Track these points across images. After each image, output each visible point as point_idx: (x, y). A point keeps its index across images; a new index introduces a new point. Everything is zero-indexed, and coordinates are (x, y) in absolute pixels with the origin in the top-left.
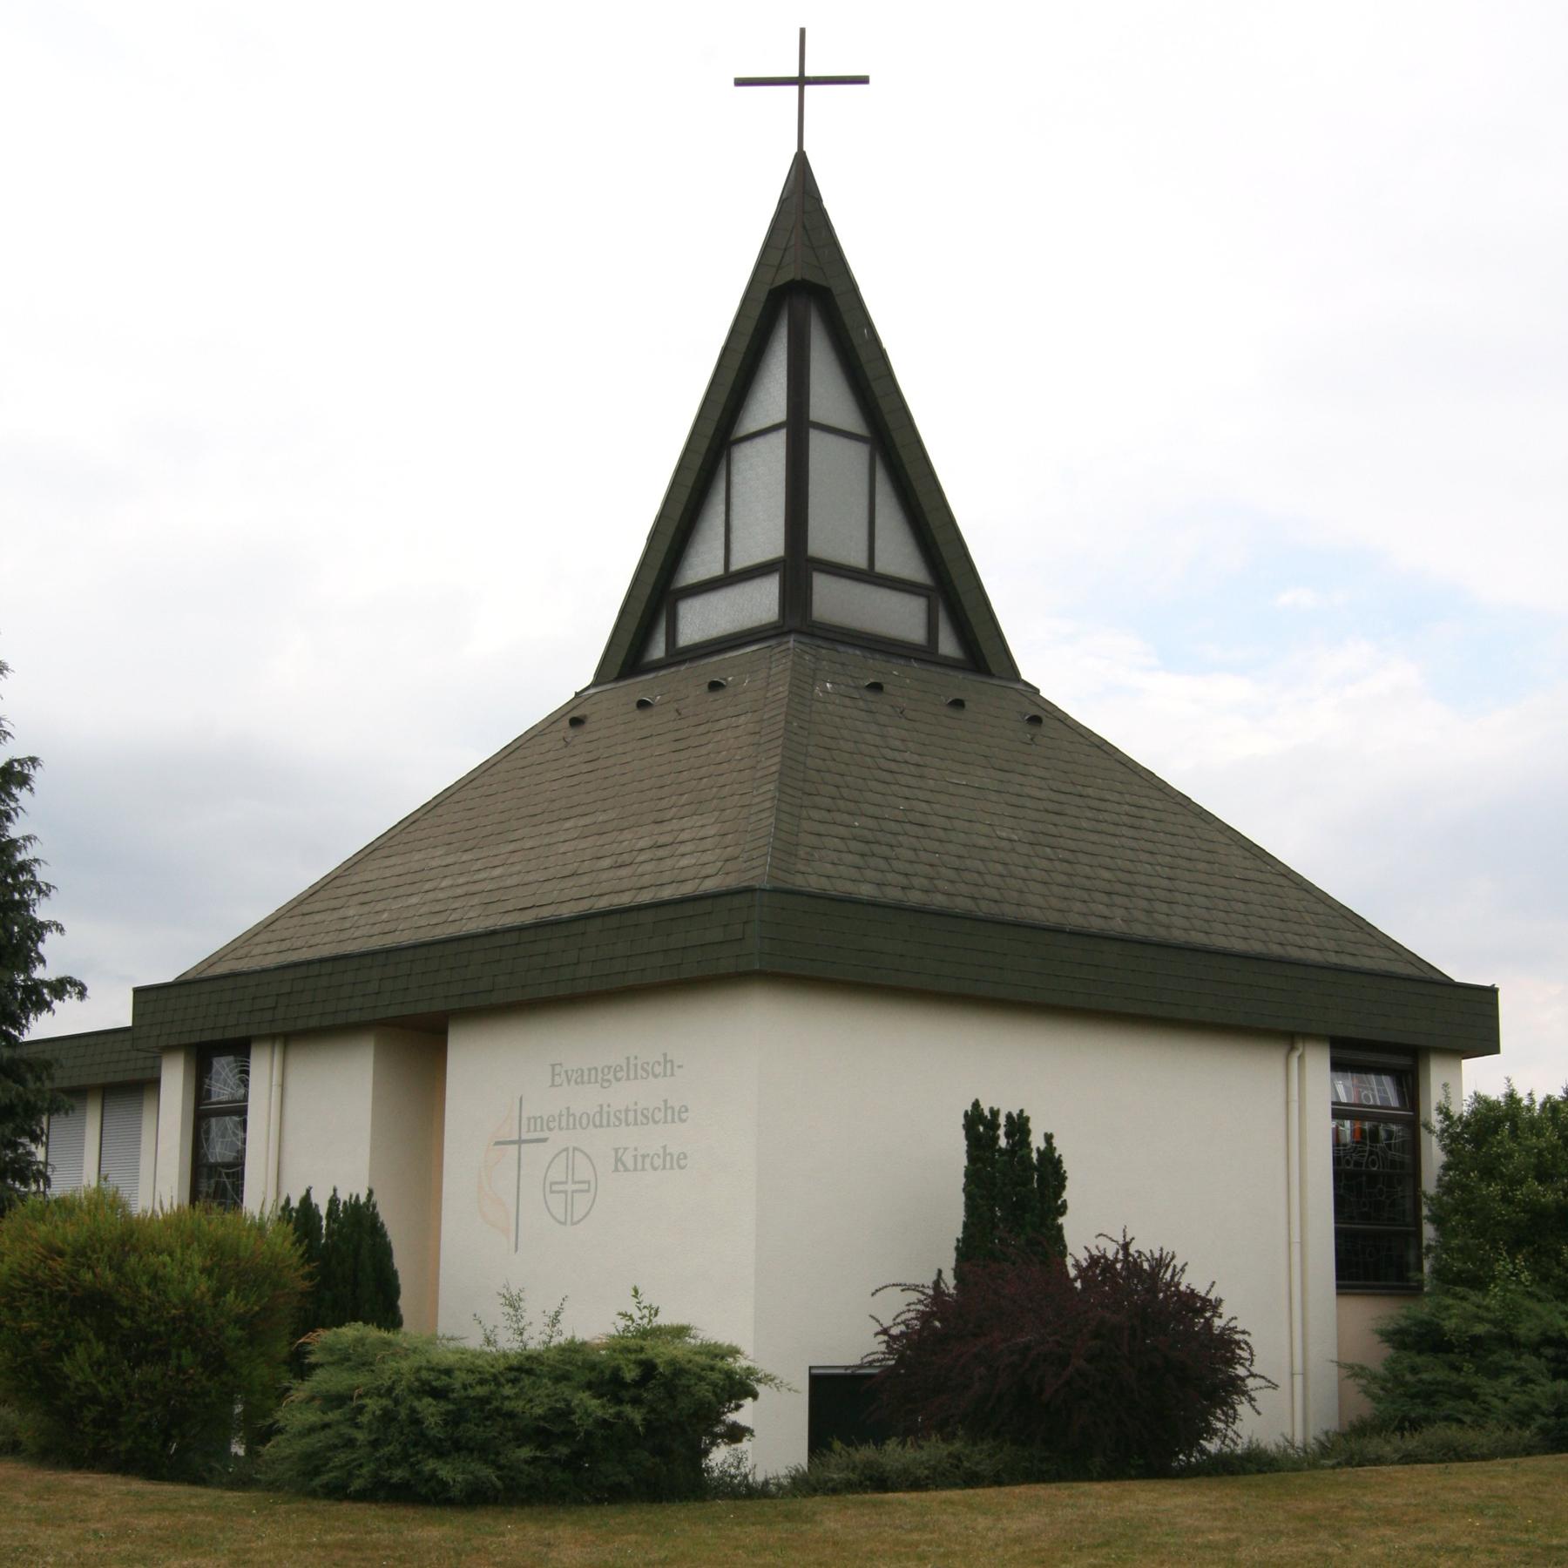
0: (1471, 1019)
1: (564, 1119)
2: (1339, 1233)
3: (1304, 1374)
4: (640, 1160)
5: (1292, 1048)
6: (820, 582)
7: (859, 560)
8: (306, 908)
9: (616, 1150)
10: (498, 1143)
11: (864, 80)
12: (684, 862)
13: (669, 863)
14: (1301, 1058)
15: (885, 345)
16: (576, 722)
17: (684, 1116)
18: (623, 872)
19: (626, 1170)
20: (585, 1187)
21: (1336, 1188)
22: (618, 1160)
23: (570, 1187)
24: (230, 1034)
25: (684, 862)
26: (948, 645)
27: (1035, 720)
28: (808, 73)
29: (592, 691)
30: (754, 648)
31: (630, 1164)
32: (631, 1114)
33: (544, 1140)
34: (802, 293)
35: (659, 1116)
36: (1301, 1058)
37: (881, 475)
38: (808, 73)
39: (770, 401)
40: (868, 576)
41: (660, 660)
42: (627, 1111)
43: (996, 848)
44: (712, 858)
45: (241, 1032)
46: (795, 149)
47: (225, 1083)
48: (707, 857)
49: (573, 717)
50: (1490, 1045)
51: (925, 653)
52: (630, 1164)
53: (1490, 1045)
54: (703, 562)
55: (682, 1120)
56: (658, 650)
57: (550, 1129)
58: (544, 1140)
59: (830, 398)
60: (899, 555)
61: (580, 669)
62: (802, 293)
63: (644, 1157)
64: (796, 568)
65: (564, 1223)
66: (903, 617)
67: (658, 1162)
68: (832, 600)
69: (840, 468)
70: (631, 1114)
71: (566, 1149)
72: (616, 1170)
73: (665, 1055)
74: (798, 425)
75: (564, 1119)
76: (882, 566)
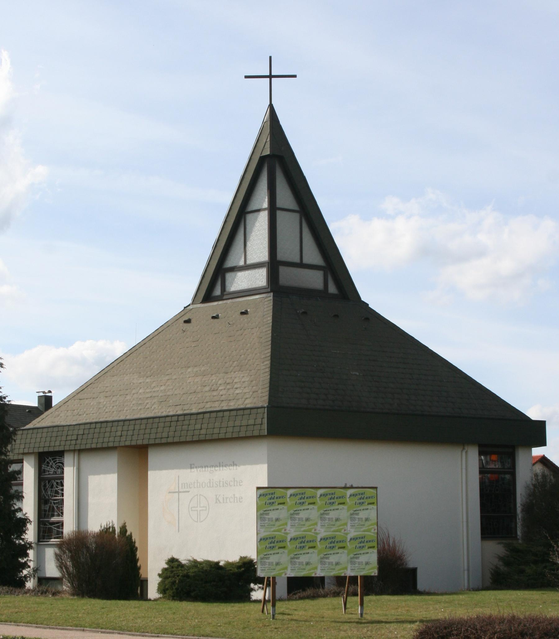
0: (536, 432)
1: (196, 484)
2: (482, 517)
3: (468, 570)
4: (225, 499)
5: (464, 449)
6: (283, 270)
7: (297, 260)
8: (80, 396)
9: (216, 496)
10: (170, 492)
11: (295, 76)
12: (237, 391)
13: (231, 391)
14: (466, 452)
15: (305, 174)
16: (188, 321)
17: (241, 484)
18: (215, 393)
19: (220, 503)
20: (204, 509)
21: (481, 500)
22: (217, 499)
23: (199, 509)
24: (57, 449)
25: (237, 391)
26: (332, 289)
27: (367, 319)
28: (273, 74)
29: (191, 307)
30: (257, 297)
31: (221, 501)
32: (221, 483)
33: (188, 492)
34: (274, 160)
35: (232, 483)
36: (466, 452)
37: (304, 225)
38: (273, 74)
39: (261, 199)
40: (301, 265)
41: (218, 296)
42: (220, 481)
43: (291, 610)
44: (248, 391)
45: (61, 448)
46: (269, 103)
47: (52, 467)
48: (246, 390)
49: (185, 319)
50: (543, 443)
51: (323, 294)
52: (221, 501)
53: (543, 443)
54: (236, 258)
55: (240, 485)
56: (217, 292)
57: (190, 488)
58: (188, 492)
59: (285, 197)
60: (312, 255)
61: (189, 301)
62: (274, 160)
63: (227, 498)
64: (274, 265)
65: (197, 522)
66: (314, 280)
67: (232, 500)
68: (287, 276)
69: (289, 223)
70: (221, 483)
71: (197, 495)
72: (216, 502)
73: (233, 462)
74: (273, 210)
75: (196, 484)
76: (306, 260)
